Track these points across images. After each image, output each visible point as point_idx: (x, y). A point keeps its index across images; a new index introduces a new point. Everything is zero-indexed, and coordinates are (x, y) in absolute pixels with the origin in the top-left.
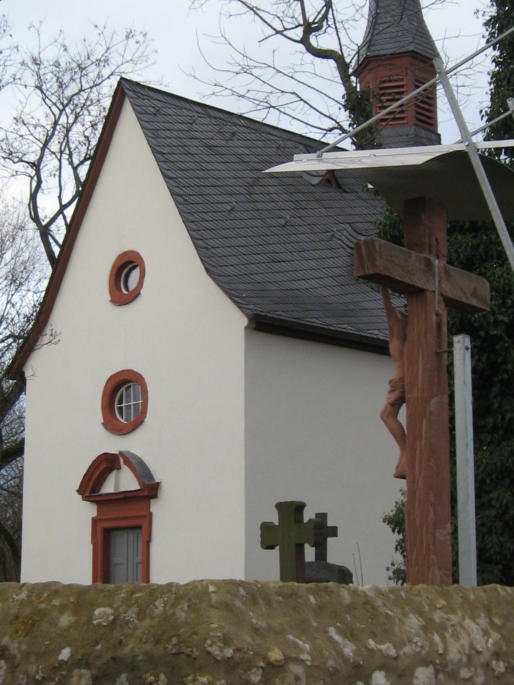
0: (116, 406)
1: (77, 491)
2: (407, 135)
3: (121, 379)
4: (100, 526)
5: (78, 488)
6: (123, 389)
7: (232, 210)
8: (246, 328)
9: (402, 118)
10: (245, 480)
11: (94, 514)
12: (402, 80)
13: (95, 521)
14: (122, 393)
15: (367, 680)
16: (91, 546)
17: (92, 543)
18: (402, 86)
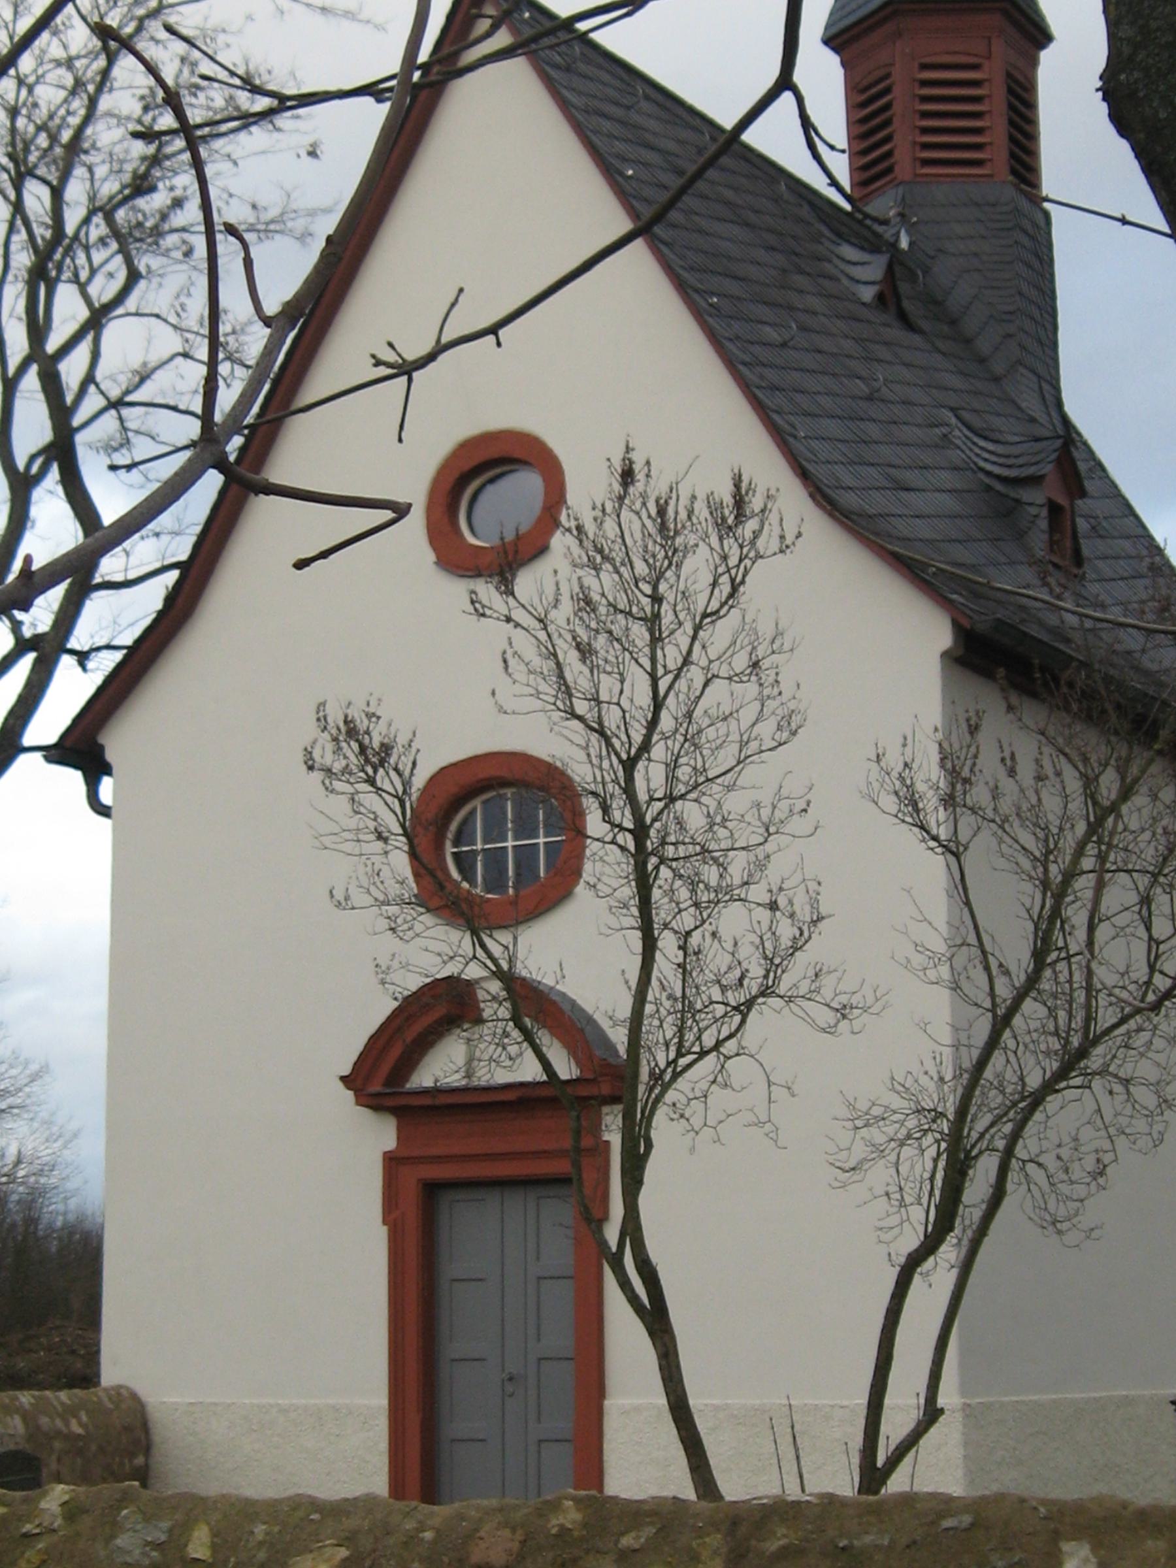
0: (449, 849)
1: (343, 1079)
2: (993, 205)
3: (481, 776)
4: (412, 1177)
5: (346, 1070)
6: (477, 803)
7: (784, 345)
8: (945, 655)
9: (978, 163)
10: (108, 1072)
11: (389, 1141)
12: (975, 67)
13: (391, 1161)
14: (472, 813)
15: (1054, 1560)
16: (384, 1231)
17: (385, 1222)
18: (976, 83)
